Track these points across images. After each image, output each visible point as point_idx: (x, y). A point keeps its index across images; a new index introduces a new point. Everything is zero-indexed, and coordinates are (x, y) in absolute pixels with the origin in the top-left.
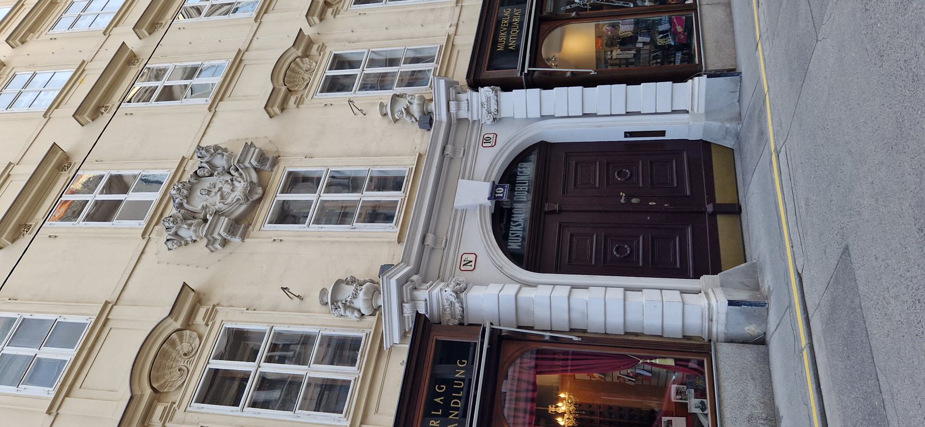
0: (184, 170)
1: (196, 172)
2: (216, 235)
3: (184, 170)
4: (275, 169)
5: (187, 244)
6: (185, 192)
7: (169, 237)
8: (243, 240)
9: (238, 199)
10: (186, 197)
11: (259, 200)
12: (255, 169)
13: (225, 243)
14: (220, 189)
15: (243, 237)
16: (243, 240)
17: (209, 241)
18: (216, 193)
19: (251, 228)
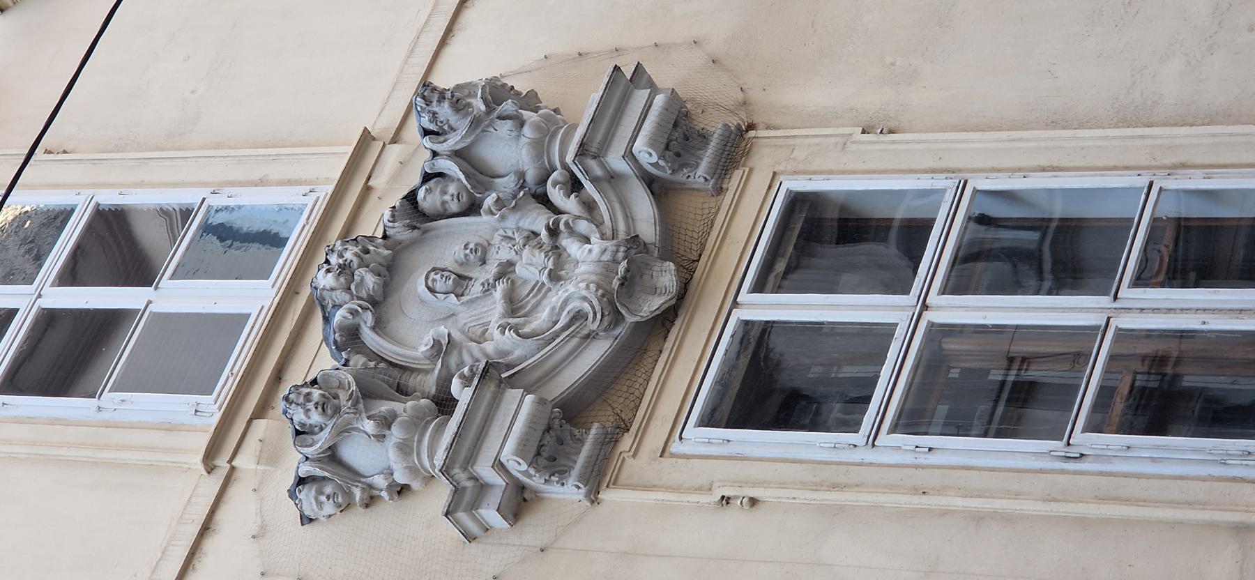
0: (367, 189)
1: (411, 197)
3: (367, 189)
6: (370, 280)
8: (593, 496)
11: (666, 319)
12: (650, 182)
13: (520, 503)
14: (506, 269)
15: (597, 479)
16: (593, 496)
17: (458, 491)
18: (488, 288)
19: (627, 442)
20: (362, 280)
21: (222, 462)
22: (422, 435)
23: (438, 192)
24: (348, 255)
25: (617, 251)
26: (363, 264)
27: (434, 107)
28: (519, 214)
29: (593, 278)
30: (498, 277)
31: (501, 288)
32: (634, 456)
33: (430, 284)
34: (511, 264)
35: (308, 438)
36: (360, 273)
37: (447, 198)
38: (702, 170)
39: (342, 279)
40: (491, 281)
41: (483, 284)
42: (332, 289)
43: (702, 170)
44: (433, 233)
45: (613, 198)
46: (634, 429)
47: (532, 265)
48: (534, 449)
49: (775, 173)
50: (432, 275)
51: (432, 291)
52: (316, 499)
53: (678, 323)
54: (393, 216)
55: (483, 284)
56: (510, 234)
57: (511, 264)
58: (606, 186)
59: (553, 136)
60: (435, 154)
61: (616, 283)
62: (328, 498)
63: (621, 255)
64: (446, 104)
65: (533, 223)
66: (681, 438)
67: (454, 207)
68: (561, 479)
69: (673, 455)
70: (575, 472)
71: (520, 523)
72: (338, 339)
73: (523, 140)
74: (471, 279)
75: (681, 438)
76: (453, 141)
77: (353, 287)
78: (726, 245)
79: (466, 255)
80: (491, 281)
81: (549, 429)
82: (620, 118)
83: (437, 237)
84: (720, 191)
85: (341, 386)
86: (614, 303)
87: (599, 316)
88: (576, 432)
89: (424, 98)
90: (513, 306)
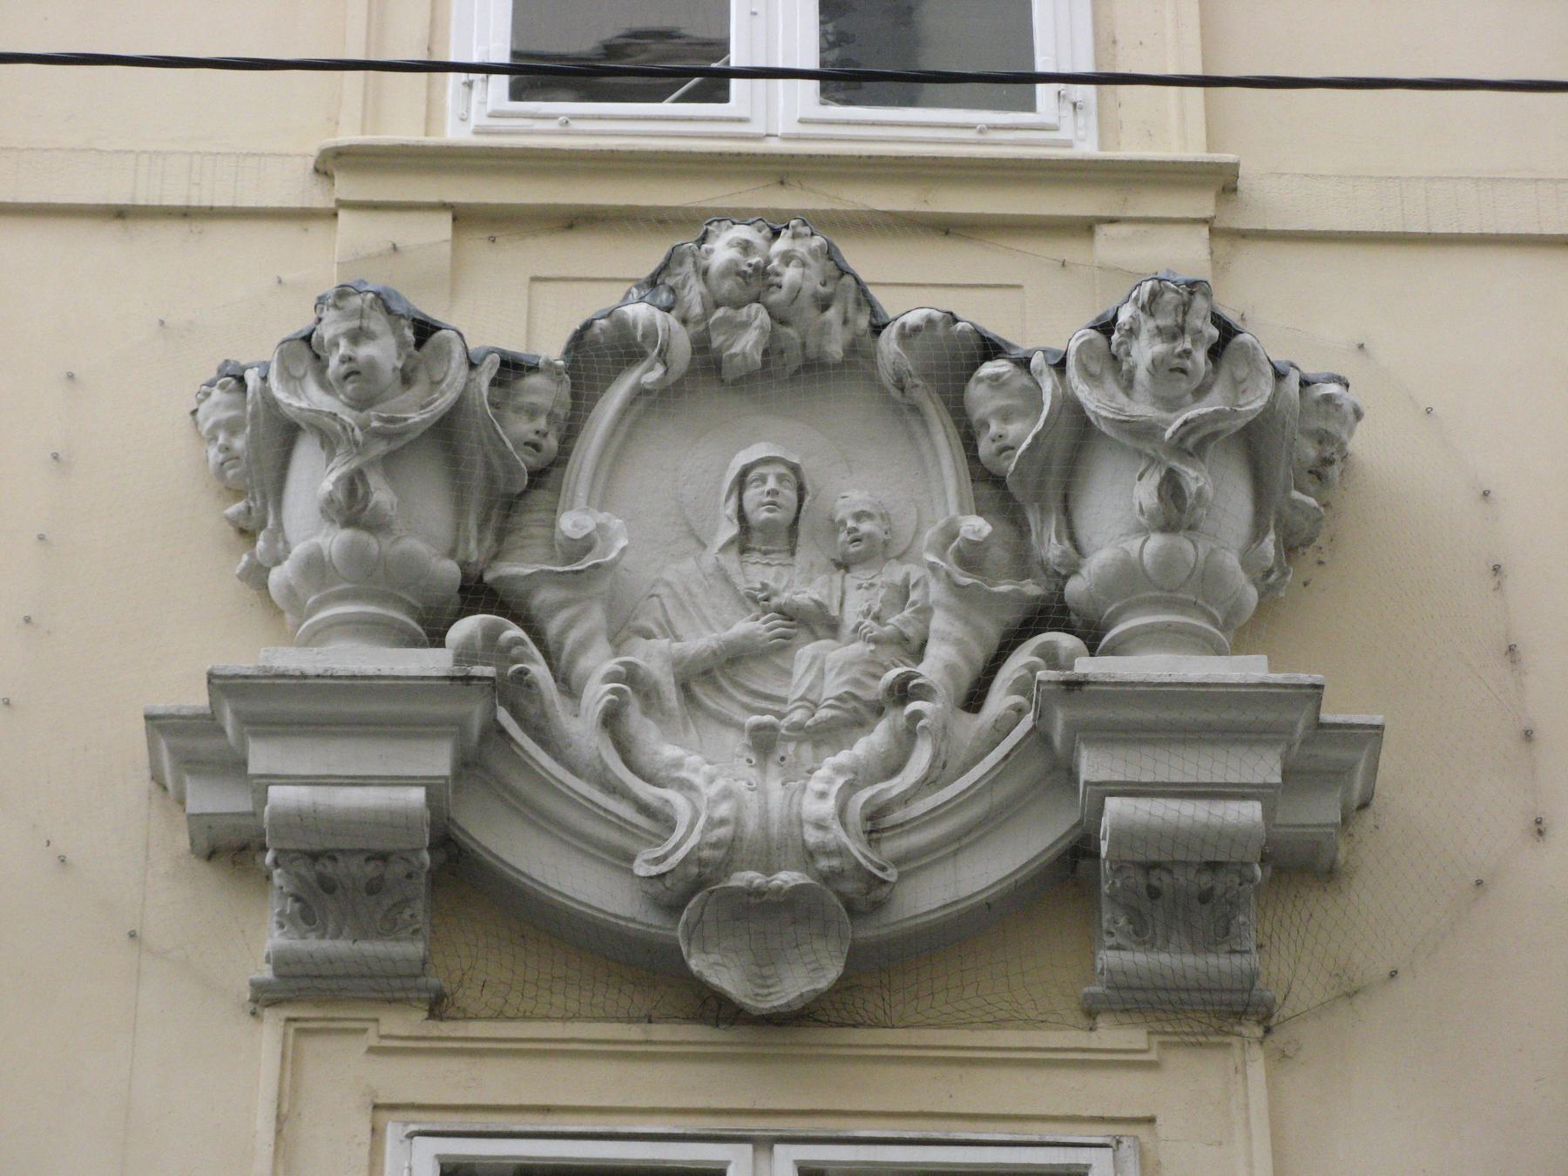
0: (1086, 228)
1: (991, 348)
2: (262, 757)
3: (1086, 228)
4: (1113, 1035)
5: (247, 533)
6: (747, 344)
7: (252, 377)
8: (264, 998)
9: (662, 819)
10: (708, 362)
11: (716, 1009)
12: (1079, 853)
13: (231, 851)
14: (816, 622)
15: (292, 990)
16: (264, 998)
17: (208, 724)
18: (759, 600)
19: (404, 1023)
20: (745, 325)
21: (348, 187)
22: (355, 596)
23: (1000, 401)
24: (791, 274)
25: (829, 854)
26: (779, 318)
27: (1147, 325)
28: (952, 601)
29: (751, 825)
30: (789, 614)
31: (744, 626)
32: (372, 1050)
33: (753, 475)
34: (833, 627)
35: (304, 366)
36: (758, 315)
37: (994, 428)
38: (1135, 959)
39: (728, 285)
40: (775, 601)
41: (764, 587)
42: (705, 273)
43: (1135, 959)
44: (917, 428)
45: (1001, 793)
46: (445, 1028)
47: (822, 672)
48: (317, 847)
49: (1151, 1120)
50: (771, 471)
51: (741, 482)
52: (217, 426)
53: (717, 1034)
54: (916, 329)
55: (764, 587)
56: (914, 596)
57: (833, 627)
58: (1035, 766)
59: (1169, 604)
60: (1060, 366)
61: (746, 877)
62: (226, 449)
63: (824, 864)
64: (1160, 347)
65: (943, 639)
66: (411, 1136)
67: (985, 448)
68: (291, 918)
69: (375, 1131)
70: (315, 945)
71: (202, 867)
72: (596, 329)
73: (1134, 545)
74: (793, 553)
75: (411, 1136)
76: (1097, 400)
77: (720, 312)
78: (937, 1071)
79: (843, 522)
80: (775, 601)
81: (383, 857)
82: (1126, 742)
83: (912, 438)
84: (1091, 1012)
85: (435, 384)
86: (694, 889)
87: (663, 868)
88: (419, 906)
89: (1154, 295)
90: (704, 677)
